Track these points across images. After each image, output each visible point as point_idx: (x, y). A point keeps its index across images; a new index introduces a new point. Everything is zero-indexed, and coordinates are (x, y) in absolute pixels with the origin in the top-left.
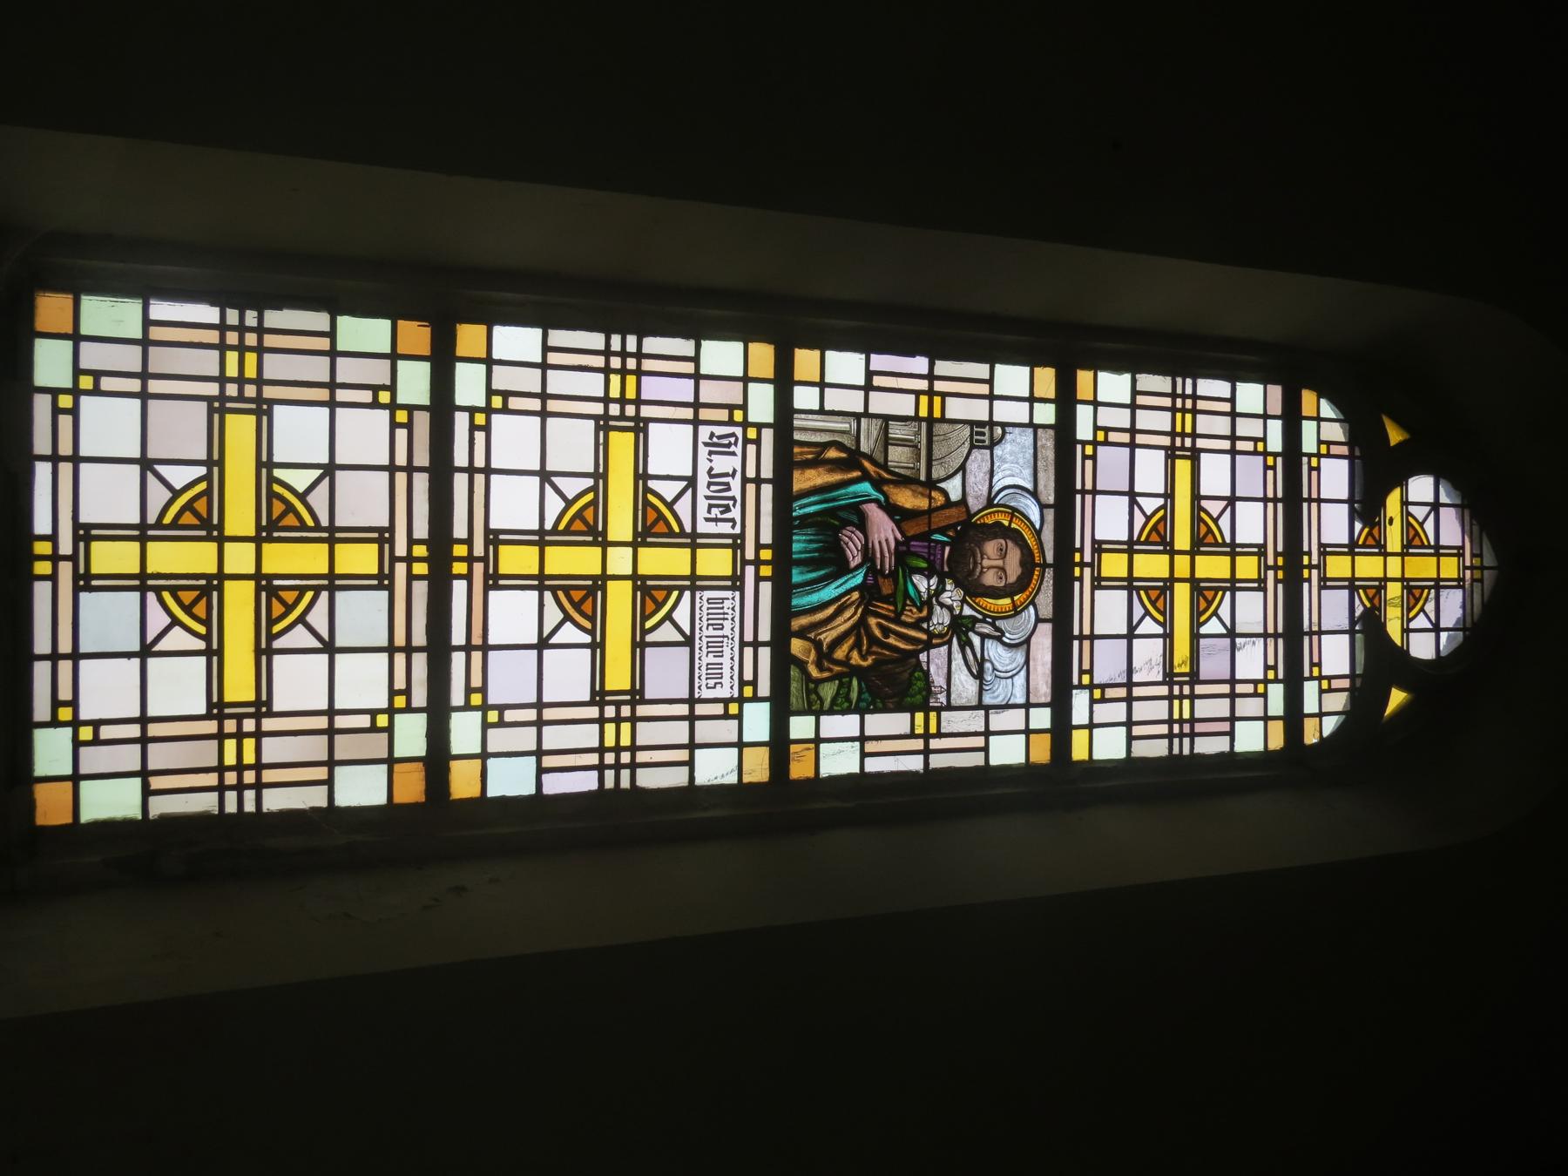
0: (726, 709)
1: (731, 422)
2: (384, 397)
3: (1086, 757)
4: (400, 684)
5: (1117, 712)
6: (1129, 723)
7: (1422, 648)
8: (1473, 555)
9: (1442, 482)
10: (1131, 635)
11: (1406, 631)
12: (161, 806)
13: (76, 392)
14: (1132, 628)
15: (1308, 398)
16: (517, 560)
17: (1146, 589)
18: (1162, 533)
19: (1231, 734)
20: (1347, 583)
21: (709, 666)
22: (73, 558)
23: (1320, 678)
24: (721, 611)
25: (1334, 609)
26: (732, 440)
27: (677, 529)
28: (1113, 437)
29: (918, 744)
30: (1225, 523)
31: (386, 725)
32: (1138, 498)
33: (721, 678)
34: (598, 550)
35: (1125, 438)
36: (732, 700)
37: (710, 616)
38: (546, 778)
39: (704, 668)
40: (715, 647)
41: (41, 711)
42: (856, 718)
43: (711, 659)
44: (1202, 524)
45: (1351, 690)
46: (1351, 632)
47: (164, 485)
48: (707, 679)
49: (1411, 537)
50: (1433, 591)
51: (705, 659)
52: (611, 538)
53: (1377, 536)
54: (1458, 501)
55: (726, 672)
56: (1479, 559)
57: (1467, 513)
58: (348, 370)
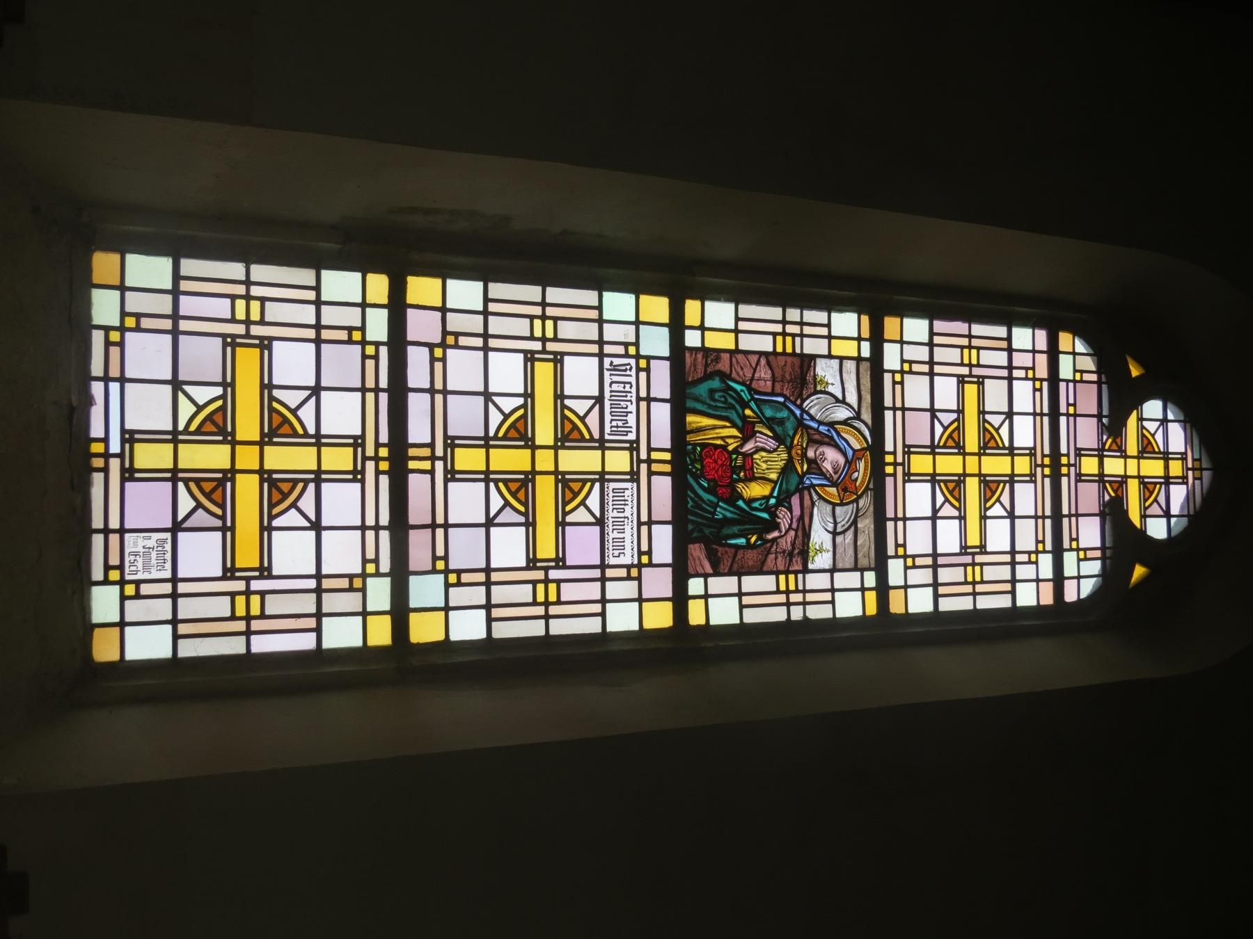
0: (629, 572)
1: (627, 355)
2: (357, 336)
3: (703, 622)
4: (370, 554)
5: (163, 609)
6: (174, 622)
7: (1157, 529)
8: (1194, 460)
9: (1169, 405)
10: (934, 518)
11: (1144, 517)
12: (188, 649)
13: (122, 329)
14: (935, 511)
15: (1065, 340)
16: (337, 459)
17: (945, 482)
18: (957, 440)
19: (318, 630)
20: (929, 478)
21: (615, 540)
22: (365, 459)
23: (1078, 550)
24: (623, 498)
25: (1090, 497)
26: (628, 367)
27: (587, 437)
28: (916, 368)
29: (240, 626)
30: (1004, 431)
31: (637, 576)
32: (937, 413)
33: (624, 549)
34: (961, 457)
35: (926, 368)
36: (632, 566)
37: (615, 503)
38: (181, 642)
39: (611, 541)
40: (620, 524)
41: (97, 574)
42: (735, 579)
43: (616, 535)
44: (987, 433)
45: (1103, 559)
46: (1102, 515)
47: (188, 399)
48: (613, 550)
49: (1144, 446)
50: (1008, 485)
51: (612, 535)
52: (538, 442)
53: (1119, 444)
54: (1182, 418)
55: (628, 545)
56: (1198, 463)
57: (1188, 426)
58: (330, 316)
